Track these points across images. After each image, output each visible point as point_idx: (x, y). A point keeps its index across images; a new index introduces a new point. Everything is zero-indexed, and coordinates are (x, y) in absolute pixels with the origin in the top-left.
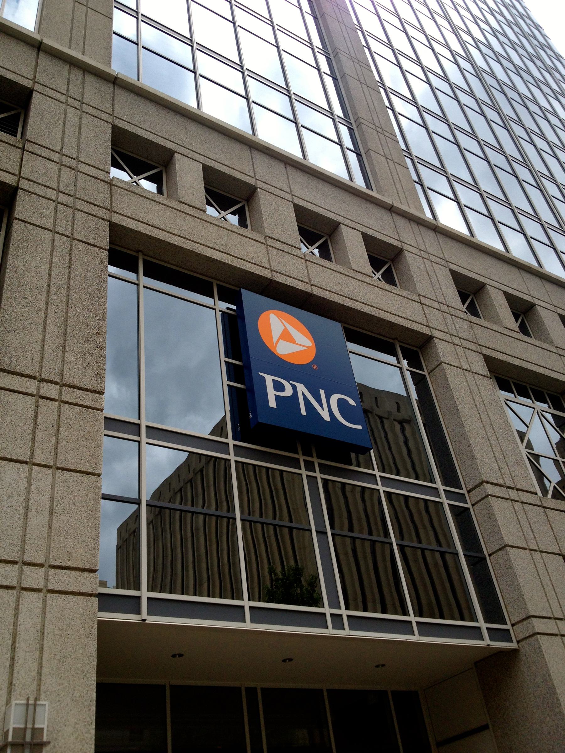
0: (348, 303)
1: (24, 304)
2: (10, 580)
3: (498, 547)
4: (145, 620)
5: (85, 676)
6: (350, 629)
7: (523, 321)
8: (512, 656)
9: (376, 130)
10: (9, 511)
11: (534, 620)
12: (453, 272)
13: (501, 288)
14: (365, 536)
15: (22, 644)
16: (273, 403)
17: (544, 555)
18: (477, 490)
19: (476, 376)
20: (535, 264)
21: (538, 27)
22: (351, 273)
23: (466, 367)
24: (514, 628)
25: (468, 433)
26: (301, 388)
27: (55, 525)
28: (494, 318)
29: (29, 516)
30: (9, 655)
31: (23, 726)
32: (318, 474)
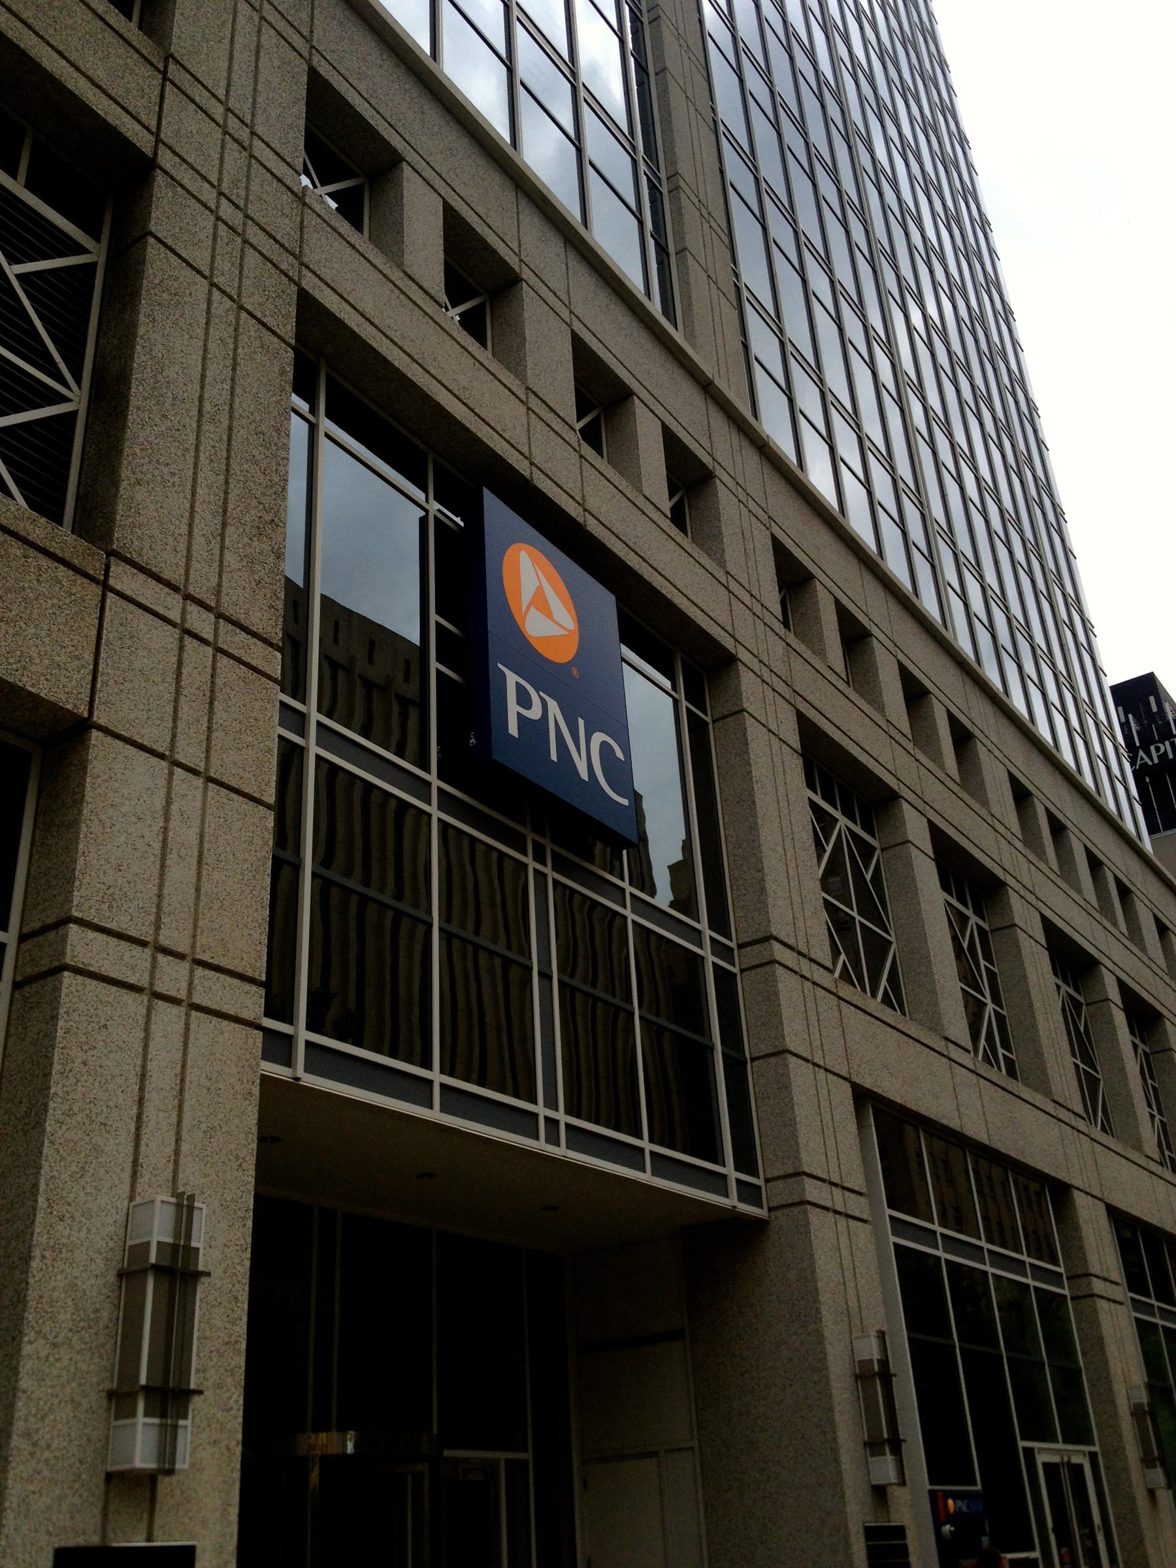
0: (632, 561)
1: (163, 428)
2: (138, 975)
3: (771, 1050)
4: (298, 1079)
5: (240, 1165)
6: (441, 1111)
7: (681, 501)
8: (759, 1226)
9: (699, 210)
10: (138, 845)
11: (806, 1179)
12: (314, 77)
13: (832, 590)
14: (386, 898)
15: (154, 1094)
16: (513, 729)
17: (830, 1076)
18: (757, 947)
19: (785, 746)
20: (504, 132)
21: (943, 64)
22: (640, 501)
23: (773, 727)
24: (770, 1185)
25: (764, 848)
26: (553, 707)
27: (206, 887)
28: (626, 462)
29: (168, 862)
30: (135, 1111)
31: (170, 1240)
32: (548, 870)
